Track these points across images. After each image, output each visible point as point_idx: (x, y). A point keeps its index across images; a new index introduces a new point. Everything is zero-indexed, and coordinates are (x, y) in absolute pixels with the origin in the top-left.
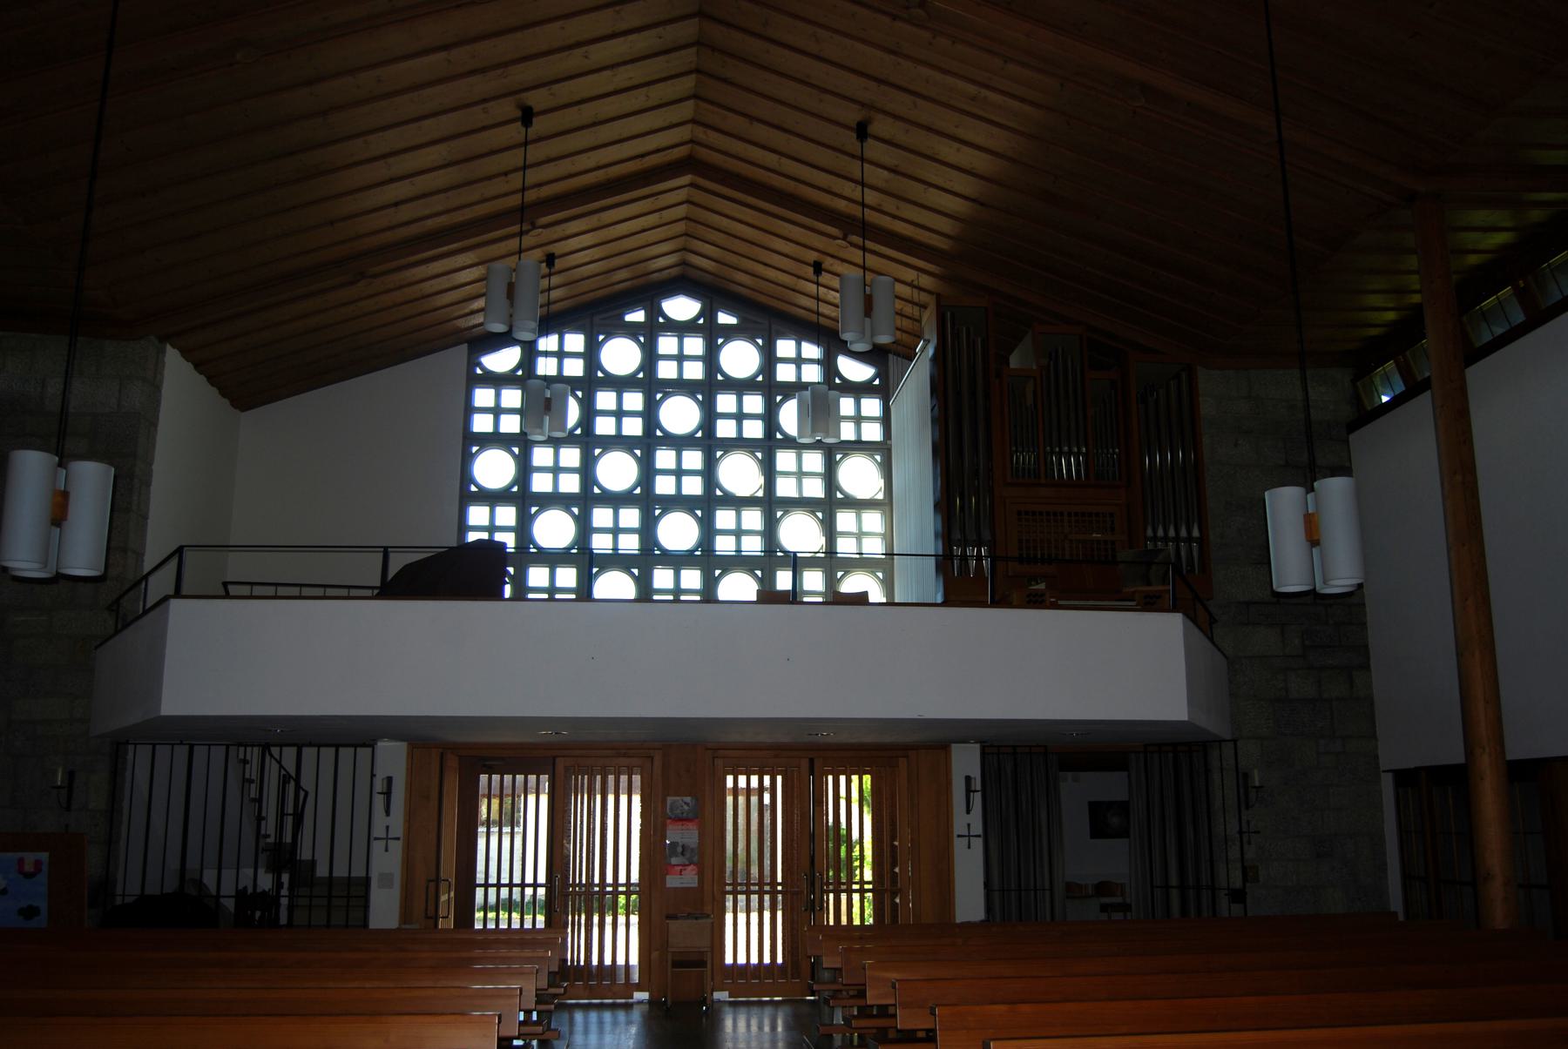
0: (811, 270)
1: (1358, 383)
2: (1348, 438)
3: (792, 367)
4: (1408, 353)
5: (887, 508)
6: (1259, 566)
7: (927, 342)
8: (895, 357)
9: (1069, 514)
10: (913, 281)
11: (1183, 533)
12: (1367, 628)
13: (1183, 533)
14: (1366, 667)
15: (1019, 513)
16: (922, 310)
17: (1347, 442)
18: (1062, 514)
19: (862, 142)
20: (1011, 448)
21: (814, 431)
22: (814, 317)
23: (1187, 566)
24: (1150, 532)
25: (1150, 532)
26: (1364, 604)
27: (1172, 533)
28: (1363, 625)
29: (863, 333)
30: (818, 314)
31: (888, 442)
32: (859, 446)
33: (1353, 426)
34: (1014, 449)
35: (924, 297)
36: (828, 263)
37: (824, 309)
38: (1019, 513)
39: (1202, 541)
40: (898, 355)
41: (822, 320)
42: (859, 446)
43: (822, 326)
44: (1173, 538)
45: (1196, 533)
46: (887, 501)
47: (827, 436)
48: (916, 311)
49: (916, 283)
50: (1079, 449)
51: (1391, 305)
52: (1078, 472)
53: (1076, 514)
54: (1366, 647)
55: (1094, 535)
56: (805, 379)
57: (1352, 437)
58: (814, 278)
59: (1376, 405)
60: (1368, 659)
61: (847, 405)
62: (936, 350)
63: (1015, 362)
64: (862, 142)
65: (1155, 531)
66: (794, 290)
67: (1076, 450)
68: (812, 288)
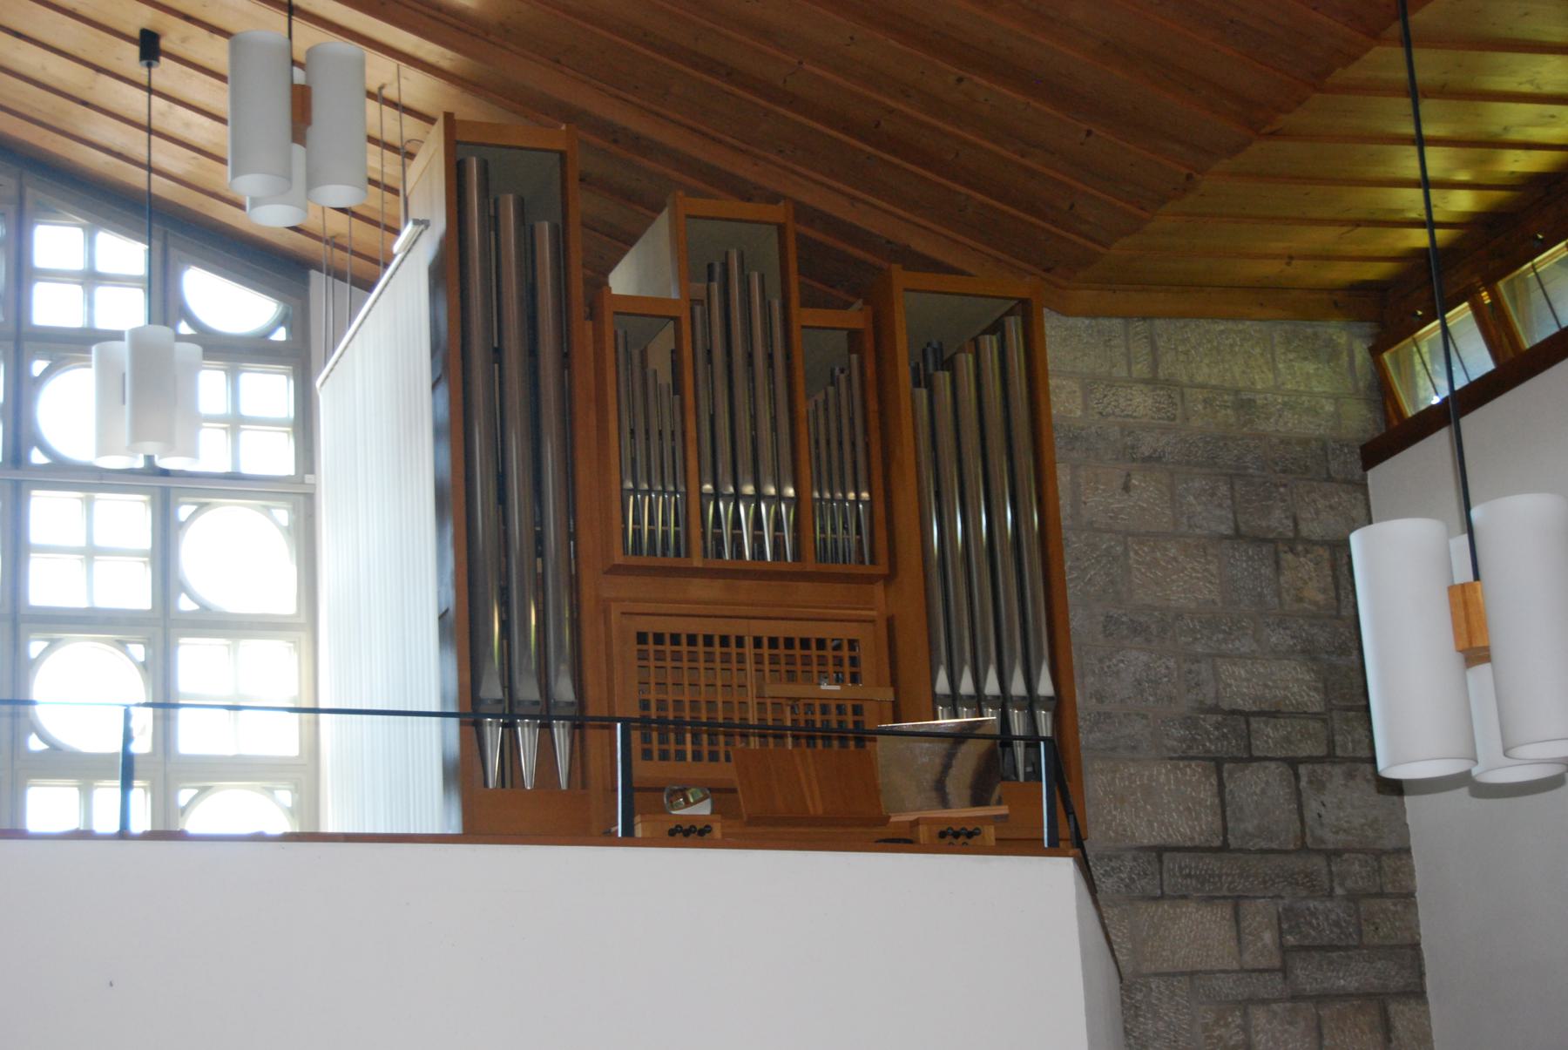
0: (133, 51)
1: (1386, 356)
2: (1364, 478)
3: (76, 291)
4: (1501, 285)
5: (304, 637)
6: (1181, 764)
7: (423, 224)
8: (330, 278)
9: (758, 642)
10: (381, 88)
11: (1018, 687)
12: (1415, 904)
13: (1018, 687)
14: (1417, 993)
15: (642, 638)
16: (407, 161)
17: (1363, 487)
18: (740, 642)
19: (149, 66)
20: (622, 482)
21: (138, 434)
22: (137, 177)
23: (1025, 767)
24: (942, 685)
25: (942, 685)
26: (1408, 851)
27: (992, 687)
28: (1408, 897)
29: (288, 177)
30: (150, 168)
31: (308, 478)
32: (234, 484)
33: (1376, 452)
34: (630, 485)
35: (412, 127)
36: (175, 35)
37: (167, 157)
38: (642, 638)
39: (1059, 705)
40: (338, 274)
41: (161, 186)
42: (234, 484)
43: (159, 198)
44: (970, 697)
45: (1045, 687)
46: (302, 620)
47: (170, 450)
48: (389, 166)
49: (390, 93)
50: (779, 489)
51: (1463, 176)
52: (758, 540)
53: (773, 642)
54: (1416, 947)
55: (825, 687)
56: (103, 323)
57: (1372, 475)
58: (138, 70)
59: (1423, 407)
60: (1422, 975)
61: (211, 386)
62: (445, 243)
63: (622, 281)
64: (149, 66)
65: (953, 682)
66: (85, 103)
67: (749, 489)
68: (133, 101)
